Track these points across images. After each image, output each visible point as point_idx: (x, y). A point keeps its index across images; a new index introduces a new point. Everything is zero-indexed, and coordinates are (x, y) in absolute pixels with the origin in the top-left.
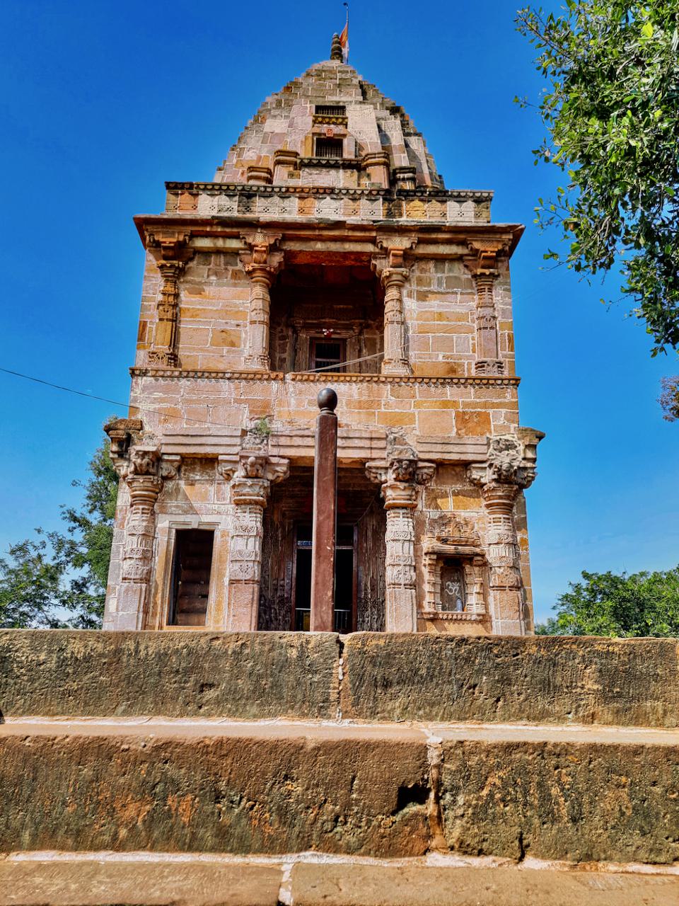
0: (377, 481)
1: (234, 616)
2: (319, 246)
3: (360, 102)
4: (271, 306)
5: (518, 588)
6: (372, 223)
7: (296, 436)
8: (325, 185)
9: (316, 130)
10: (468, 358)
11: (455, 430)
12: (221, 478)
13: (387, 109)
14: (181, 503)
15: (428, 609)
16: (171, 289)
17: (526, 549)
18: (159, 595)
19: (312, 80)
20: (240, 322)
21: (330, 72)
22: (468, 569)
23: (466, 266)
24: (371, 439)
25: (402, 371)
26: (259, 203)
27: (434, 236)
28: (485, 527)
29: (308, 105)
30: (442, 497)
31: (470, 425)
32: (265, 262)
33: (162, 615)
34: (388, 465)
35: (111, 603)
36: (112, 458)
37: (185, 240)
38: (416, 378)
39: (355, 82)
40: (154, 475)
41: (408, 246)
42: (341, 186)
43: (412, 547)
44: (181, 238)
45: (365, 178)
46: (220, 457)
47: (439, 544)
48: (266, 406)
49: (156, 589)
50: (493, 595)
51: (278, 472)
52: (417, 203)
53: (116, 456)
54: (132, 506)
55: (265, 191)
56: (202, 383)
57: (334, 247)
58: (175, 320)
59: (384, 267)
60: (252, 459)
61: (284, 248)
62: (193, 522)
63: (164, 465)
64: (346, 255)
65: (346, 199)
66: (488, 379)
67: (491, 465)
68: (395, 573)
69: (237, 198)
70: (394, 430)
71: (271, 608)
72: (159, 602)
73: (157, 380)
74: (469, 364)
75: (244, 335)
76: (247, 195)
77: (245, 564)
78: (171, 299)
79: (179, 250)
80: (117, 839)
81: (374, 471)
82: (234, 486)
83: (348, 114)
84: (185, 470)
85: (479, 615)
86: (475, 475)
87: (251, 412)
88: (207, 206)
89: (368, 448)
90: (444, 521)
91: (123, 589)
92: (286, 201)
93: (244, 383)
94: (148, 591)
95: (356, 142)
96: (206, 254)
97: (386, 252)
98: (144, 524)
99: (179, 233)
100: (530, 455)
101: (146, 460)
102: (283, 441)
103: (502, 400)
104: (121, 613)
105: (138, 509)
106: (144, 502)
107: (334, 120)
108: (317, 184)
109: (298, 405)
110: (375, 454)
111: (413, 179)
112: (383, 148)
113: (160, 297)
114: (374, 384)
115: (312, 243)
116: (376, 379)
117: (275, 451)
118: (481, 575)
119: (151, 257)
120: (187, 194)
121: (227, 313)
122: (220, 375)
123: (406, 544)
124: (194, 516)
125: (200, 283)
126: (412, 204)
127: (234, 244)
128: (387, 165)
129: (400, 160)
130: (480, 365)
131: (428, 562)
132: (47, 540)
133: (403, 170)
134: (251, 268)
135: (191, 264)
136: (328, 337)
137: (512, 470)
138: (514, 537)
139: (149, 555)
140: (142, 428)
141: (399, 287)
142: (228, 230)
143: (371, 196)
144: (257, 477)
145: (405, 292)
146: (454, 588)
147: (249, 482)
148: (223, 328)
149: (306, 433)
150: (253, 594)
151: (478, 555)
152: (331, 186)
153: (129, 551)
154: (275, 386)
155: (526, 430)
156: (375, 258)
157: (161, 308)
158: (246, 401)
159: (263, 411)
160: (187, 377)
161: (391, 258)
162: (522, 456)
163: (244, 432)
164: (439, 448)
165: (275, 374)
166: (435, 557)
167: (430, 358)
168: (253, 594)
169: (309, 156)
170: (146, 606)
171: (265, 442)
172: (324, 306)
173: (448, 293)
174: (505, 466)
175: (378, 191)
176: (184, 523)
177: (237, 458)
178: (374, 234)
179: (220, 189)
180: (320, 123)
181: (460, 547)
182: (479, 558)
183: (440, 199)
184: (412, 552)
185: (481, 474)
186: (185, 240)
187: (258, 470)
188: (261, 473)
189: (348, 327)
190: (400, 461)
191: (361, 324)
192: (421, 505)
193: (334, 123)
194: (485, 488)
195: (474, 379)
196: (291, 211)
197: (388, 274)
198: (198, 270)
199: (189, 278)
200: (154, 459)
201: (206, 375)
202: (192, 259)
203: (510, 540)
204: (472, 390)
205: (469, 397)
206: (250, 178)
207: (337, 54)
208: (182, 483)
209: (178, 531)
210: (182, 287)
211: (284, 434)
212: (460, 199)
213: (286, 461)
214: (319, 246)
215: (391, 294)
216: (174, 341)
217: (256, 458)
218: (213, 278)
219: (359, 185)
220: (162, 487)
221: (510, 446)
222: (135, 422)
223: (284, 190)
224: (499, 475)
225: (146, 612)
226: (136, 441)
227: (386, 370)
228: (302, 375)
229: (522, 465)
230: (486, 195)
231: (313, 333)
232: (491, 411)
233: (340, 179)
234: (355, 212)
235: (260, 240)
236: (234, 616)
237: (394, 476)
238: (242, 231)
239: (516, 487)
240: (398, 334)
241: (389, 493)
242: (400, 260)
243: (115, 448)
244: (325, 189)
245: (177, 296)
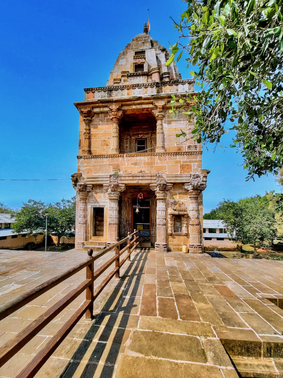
0: (153, 190)
2: (134, 107)
3: (150, 48)
4: (119, 131)
5: (198, 225)
6: (151, 96)
7: (127, 176)
8: (136, 83)
9: (135, 62)
11: (180, 171)
13: (160, 50)
14: (94, 199)
15: (169, 232)
16: (88, 128)
17: (202, 212)
18: (90, 228)
19: (134, 42)
21: (141, 38)
22: (182, 219)
24: (151, 176)
25: (162, 151)
26: (114, 93)
28: (188, 204)
29: (132, 52)
30: (175, 195)
31: (185, 169)
32: (116, 115)
33: (91, 233)
34: (157, 185)
37: (90, 110)
38: (167, 153)
39: (149, 40)
41: (164, 104)
42: (141, 83)
43: (165, 212)
44: (89, 109)
45: (150, 79)
46: (104, 185)
47: (173, 211)
48: (118, 166)
49: (89, 226)
50: (190, 227)
52: (168, 86)
55: (116, 88)
56: (98, 160)
57: (139, 107)
58: (89, 138)
59: (156, 113)
60: (112, 186)
61: (122, 109)
63: (88, 188)
64: (143, 109)
65: (143, 88)
66: (192, 152)
67: (191, 184)
68: (159, 221)
69: (107, 92)
70: (160, 172)
71: (125, 227)
72: (90, 230)
73: (85, 159)
74: (185, 147)
75: (111, 142)
76: (110, 90)
77: (113, 219)
78: (88, 131)
79: (89, 113)
81: (152, 187)
82: (108, 194)
83: (146, 54)
85: (185, 234)
86: (186, 187)
87: (113, 168)
88: (98, 96)
89: (150, 180)
90: (175, 203)
92: (123, 91)
93: (111, 158)
94: (86, 227)
95: (149, 65)
96: (98, 114)
97: (156, 107)
98: (84, 207)
99: (88, 107)
100: (204, 180)
101: (82, 187)
102: (123, 178)
103: (196, 160)
107: (140, 57)
108: (133, 83)
109: (128, 165)
110: (153, 181)
111: (169, 77)
112: (158, 66)
113: (84, 131)
114: (153, 156)
115: (131, 106)
116: (153, 154)
117: (120, 182)
118: (187, 221)
119: (81, 117)
120: (91, 92)
121: (105, 134)
122: (103, 156)
123: (163, 212)
125: (97, 124)
126: (166, 87)
127: (106, 109)
128: (159, 72)
129: (164, 70)
130: (189, 147)
131: (170, 217)
133: (165, 73)
134: (112, 118)
135: (93, 118)
136: (141, 138)
137: (198, 186)
138: (198, 208)
139: (86, 216)
140: (81, 176)
141: (161, 120)
142: (103, 104)
143: (152, 86)
144: (115, 191)
145: (163, 121)
146: (178, 224)
147: (113, 193)
148: (104, 139)
149: (130, 175)
151: (186, 215)
152: (138, 83)
154: (120, 159)
155: (204, 170)
156: (153, 110)
157: (85, 134)
158: (111, 165)
159: (117, 168)
160: (93, 158)
161: (158, 109)
162: (202, 180)
163: (111, 176)
164: (174, 178)
165: (120, 155)
166: (172, 216)
167: (172, 144)
169: (132, 72)
172: (137, 128)
173: (178, 120)
174: (196, 185)
175: (154, 83)
176: (95, 206)
177: (108, 185)
178: (152, 101)
179: (101, 89)
180: (136, 59)
181: (180, 212)
182: (186, 215)
183: (176, 84)
184: (164, 215)
185: (188, 187)
186: (90, 110)
188: (116, 190)
189: (147, 134)
190: (160, 184)
191: (151, 133)
192: (168, 198)
193: (140, 58)
194: (189, 192)
195: (187, 153)
196: (124, 95)
197: (157, 115)
198: (96, 119)
199: (93, 123)
201: (99, 156)
202: (94, 116)
203: (197, 209)
204: (186, 156)
205: (183, 159)
206: (115, 83)
207: (146, 31)
209: (94, 208)
210: (91, 126)
213: (124, 185)
214: (134, 107)
215: (159, 122)
216: (90, 146)
217: (114, 185)
218: (101, 122)
219: (148, 82)
221: (198, 177)
222: (79, 174)
223: (122, 87)
224: (194, 188)
225: (86, 233)
226: (79, 180)
227: (158, 151)
228: (129, 154)
229: (202, 183)
230: (192, 80)
231: (136, 137)
232: (192, 164)
233: (141, 80)
234: (146, 93)
235: (114, 107)
237: (159, 189)
238: (108, 104)
239: (199, 191)
240: (161, 137)
241: (157, 195)
242: (161, 110)
244: (136, 85)
245: (90, 130)
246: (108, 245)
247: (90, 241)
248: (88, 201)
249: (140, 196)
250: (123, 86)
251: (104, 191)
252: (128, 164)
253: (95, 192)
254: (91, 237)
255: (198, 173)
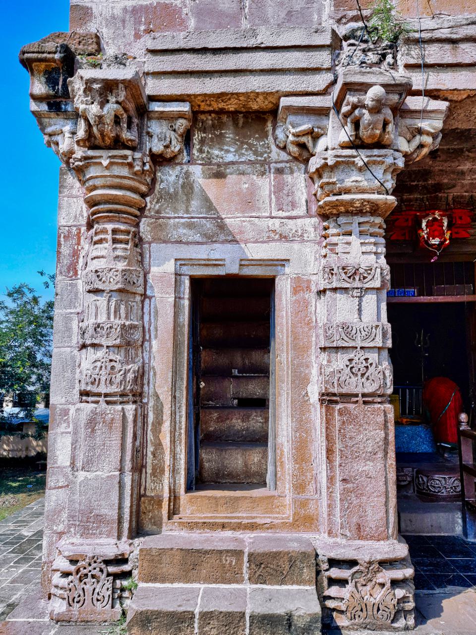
1: (344, 480)
12: (284, 156)
18: (166, 426)
33: (174, 471)
35: (59, 445)
36: (33, 112)
40: (133, 149)
46: (284, 102)
49: (159, 412)
51: (420, 132)
53: (44, 107)
54: (90, 226)
62: (227, 260)
63: (155, 127)
72: (166, 441)
77: (362, 355)
80: (124, 289)
84: (202, 142)
91: (83, 418)
94: (141, 418)
101: (111, 108)
102: (434, 54)
104: (82, 475)
105: (104, 231)
106: (115, 215)
124: (229, 246)
132: (49, 281)
140: (99, 50)
147: (361, 157)
150: (386, 427)
153: (91, 331)
168: (386, 427)
170: (139, 453)
171: (389, 59)
187: (386, 124)
200: (131, 106)
208: (196, 171)
209: (195, 282)
211: (437, 34)
220: (154, 181)
225: (139, 468)
236: (344, 480)
243: (39, 87)
246: (335, 573)
247: (172, 535)
248: (158, 227)
249: (434, 225)
251: (275, 153)
253: (208, 162)
254: (174, 498)
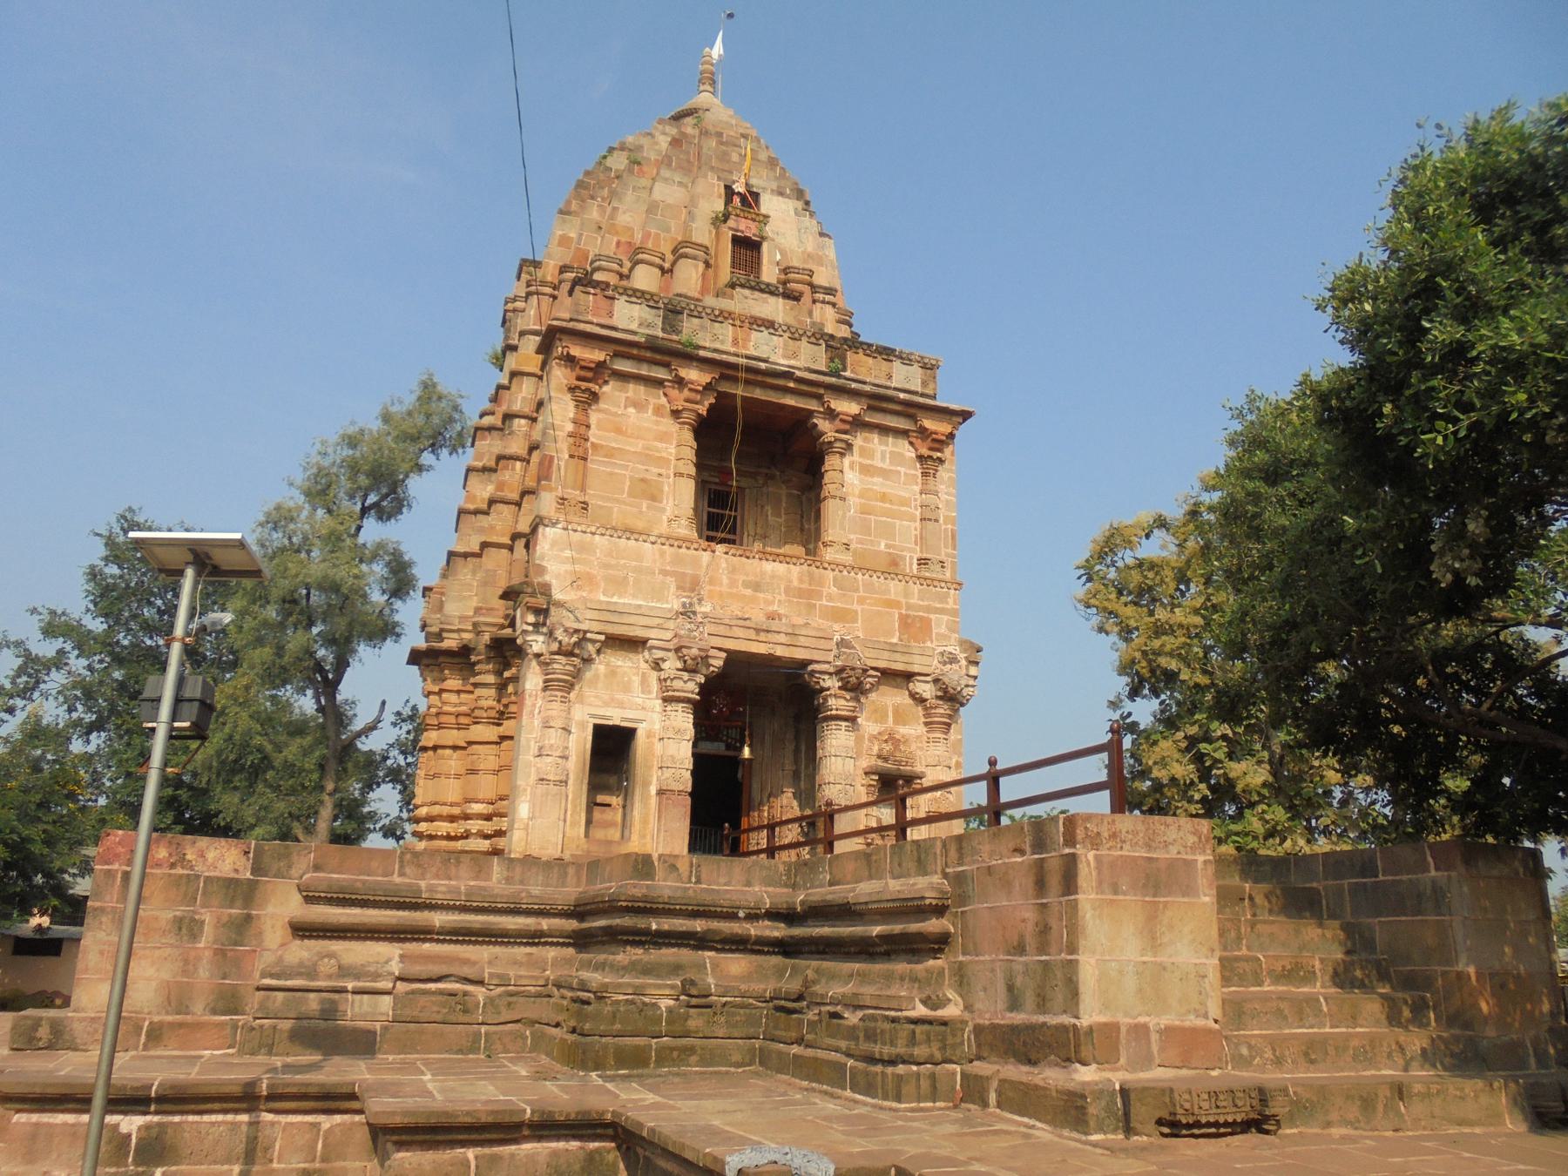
10: (910, 550)
20: (662, 471)
23: (911, 443)
27: (885, 405)
62: (616, 717)
87: (678, 588)
97: (831, 414)
142: (658, 357)
147: (686, 676)
149: (747, 623)
154: (706, 556)
164: (886, 655)
176: (603, 717)
198: (609, 389)
199: (602, 405)
212: (906, 359)
213: (724, 655)
215: (831, 462)
232: (932, 616)
234: (795, 355)
241: (832, 702)
250: (721, 312)
252: (733, 583)
255: (950, 649)
